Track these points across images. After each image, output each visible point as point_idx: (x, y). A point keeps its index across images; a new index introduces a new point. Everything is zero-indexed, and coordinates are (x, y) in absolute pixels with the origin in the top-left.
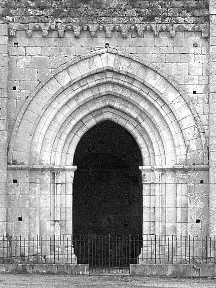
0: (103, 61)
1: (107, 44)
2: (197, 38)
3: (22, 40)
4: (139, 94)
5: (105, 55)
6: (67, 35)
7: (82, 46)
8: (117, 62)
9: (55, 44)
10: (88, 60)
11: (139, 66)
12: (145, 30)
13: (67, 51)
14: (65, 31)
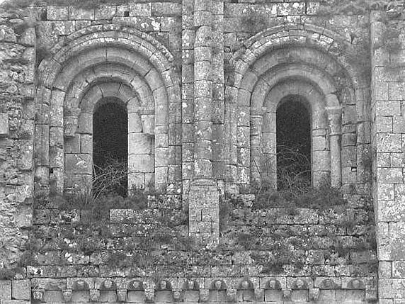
12: (268, 288)
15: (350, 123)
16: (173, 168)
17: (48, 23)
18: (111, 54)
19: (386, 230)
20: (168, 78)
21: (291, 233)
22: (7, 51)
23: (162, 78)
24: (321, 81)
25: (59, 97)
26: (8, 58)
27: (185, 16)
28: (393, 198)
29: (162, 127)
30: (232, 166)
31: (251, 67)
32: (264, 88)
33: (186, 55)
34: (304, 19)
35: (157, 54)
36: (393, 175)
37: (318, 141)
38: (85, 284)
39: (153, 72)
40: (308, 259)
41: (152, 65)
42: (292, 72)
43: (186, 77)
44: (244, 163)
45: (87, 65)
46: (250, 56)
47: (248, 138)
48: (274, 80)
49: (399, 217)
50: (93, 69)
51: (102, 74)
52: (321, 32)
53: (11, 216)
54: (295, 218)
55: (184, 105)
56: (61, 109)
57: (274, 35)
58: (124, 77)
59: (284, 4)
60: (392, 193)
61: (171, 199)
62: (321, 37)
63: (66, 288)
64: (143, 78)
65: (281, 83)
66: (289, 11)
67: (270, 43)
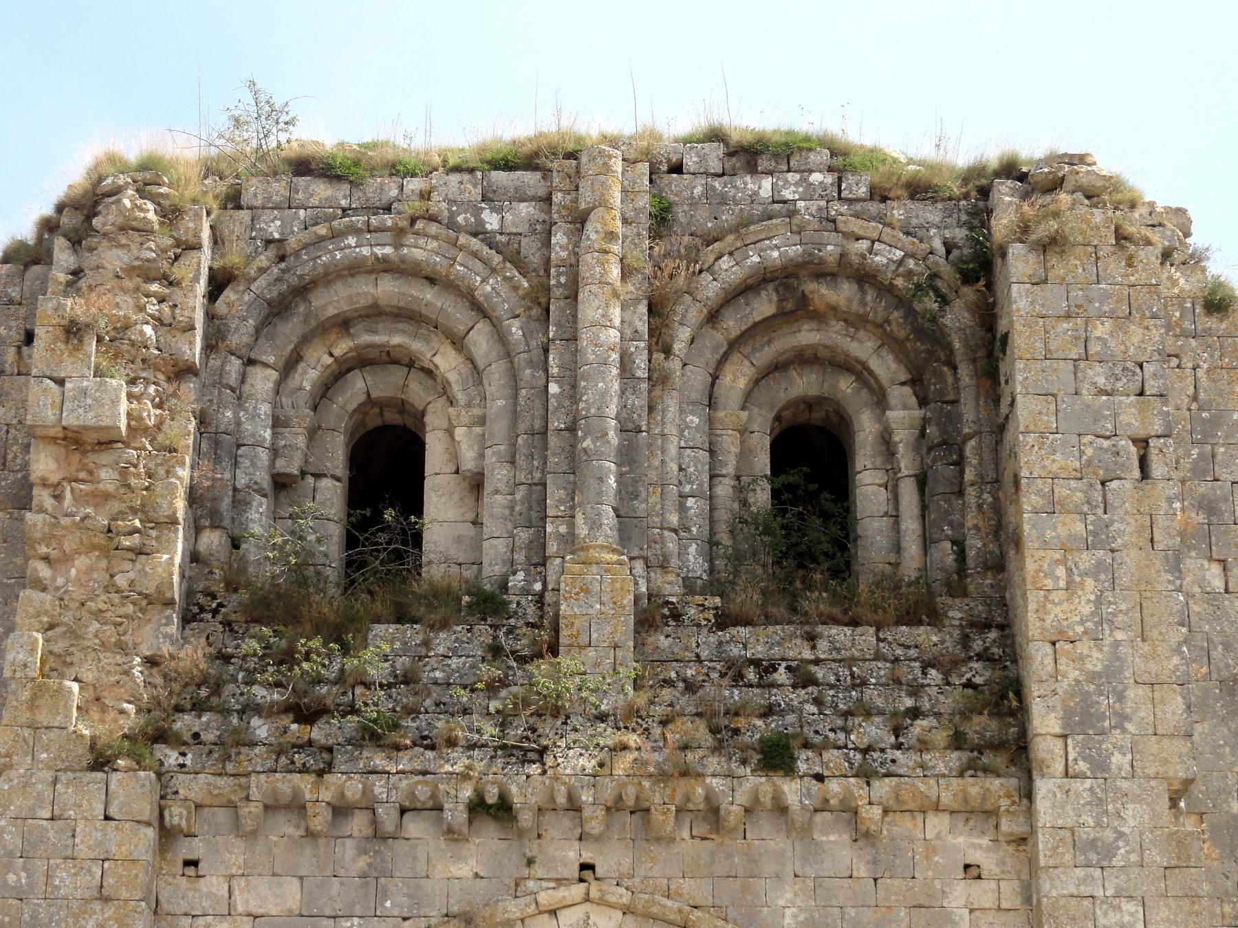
1: (585, 867)
2: (977, 841)
3: (223, 855)
4: (516, 389)
6: (415, 827)
7: (477, 875)
13: (409, 896)
14: (403, 811)
15: (945, 442)
16: (524, 535)
17: (245, 215)
18: (387, 289)
19: (1049, 661)
21: (809, 681)
22: (133, 247)
23: (501, 337)
24: (875, 357)
25: (262, 381)
26: (137, 263)
28: (1062, 584)
29: (502, 447)
30: (666, 533)
31: (713, 317)
32: (737, 378)
33: (557, 279)
34: (836, 207)
36: (1062, 531)
37: (869, 487)
38: (296, 794)
39: (482, 326)
40: (853, 737)
41: (481, 310)
42: (807, 336)
43: (559, 325)
44: (694, 530)
45: (331, 311)
46: (710, 288)
47: (706, 479)
48: (766, 355)
49: (1080, 629)
50: (344, 324)
51: (366, 338)
53: (121, 624)
55: (554, 388)
56: (265, 409)
57: (767, 242)
58: (416, 346)
60: (1061, 572)
61: (518, 603)
62: (877, 245)
63: (247, 798)
64: (458, 343)
65: (778, 367)
66: (801, 189)
67: (756, 259)
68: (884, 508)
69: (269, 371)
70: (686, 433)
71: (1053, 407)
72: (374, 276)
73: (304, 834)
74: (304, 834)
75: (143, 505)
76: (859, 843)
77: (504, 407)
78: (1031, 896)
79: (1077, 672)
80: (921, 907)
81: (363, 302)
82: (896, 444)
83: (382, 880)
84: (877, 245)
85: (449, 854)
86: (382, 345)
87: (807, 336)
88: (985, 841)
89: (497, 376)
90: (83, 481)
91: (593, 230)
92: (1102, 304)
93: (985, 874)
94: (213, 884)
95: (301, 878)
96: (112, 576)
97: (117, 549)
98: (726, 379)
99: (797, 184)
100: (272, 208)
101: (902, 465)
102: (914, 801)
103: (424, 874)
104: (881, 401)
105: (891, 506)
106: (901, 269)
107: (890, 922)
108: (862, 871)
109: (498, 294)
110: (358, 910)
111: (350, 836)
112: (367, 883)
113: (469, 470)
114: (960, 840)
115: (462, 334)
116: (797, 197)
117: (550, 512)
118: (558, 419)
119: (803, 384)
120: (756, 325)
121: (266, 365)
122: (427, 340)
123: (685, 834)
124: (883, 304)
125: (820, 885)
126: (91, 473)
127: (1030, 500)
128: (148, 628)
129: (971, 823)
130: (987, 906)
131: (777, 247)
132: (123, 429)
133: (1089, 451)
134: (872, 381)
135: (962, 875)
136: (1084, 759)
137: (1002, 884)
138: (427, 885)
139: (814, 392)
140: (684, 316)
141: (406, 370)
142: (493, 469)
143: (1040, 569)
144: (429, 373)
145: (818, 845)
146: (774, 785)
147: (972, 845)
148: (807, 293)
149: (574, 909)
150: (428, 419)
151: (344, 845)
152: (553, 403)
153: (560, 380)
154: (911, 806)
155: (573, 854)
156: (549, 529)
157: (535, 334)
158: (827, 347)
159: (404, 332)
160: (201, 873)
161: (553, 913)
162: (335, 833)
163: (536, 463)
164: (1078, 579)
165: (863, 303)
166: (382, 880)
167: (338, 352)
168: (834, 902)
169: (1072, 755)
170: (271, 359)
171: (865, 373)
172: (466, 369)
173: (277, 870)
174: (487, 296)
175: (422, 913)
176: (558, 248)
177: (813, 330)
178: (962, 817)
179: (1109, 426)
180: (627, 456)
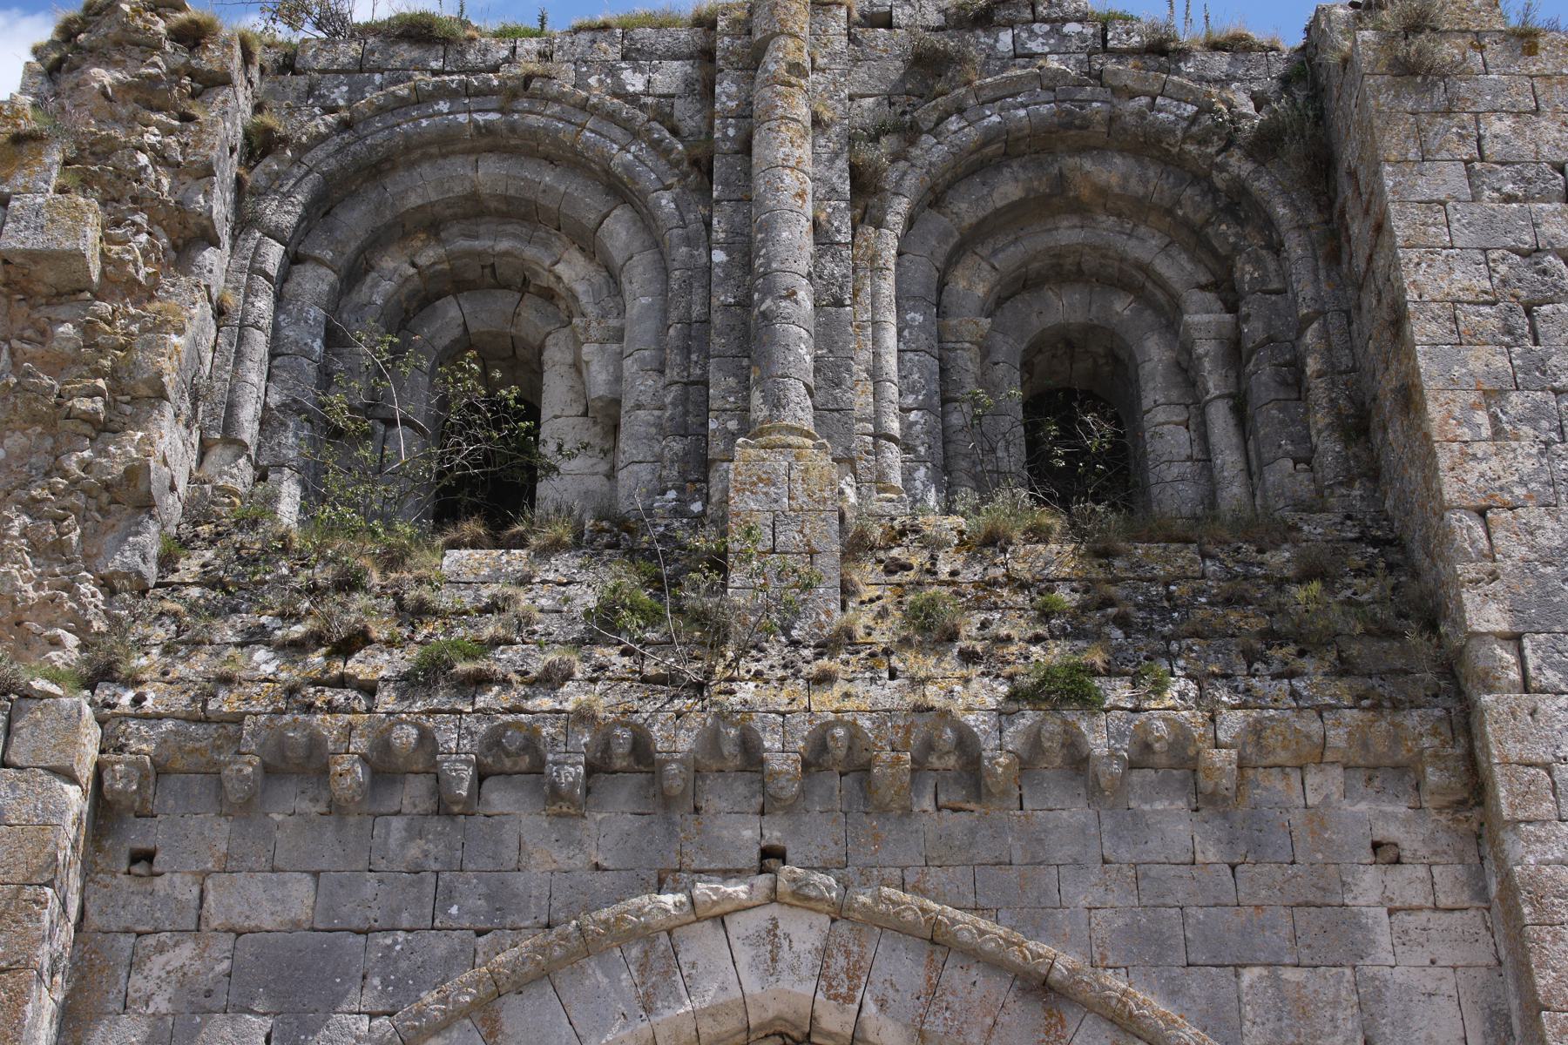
0: (744, 955)
2: (1389, 808)
5: (756, 921)
6: (499, 798)
7: (597, 867)
8: (842, 961)
9: (414, 851)
10: (635, 952)
11: (997, 988)
12: (1027, 763)
13: (489, 897)
15: (1270, 339)
18: (490, 174)
20: (666, 202)
23: (646, 219)
27: (726, 39)
28: (1486, 432)
29: (647, 353)
31: (934, 198)
32: (973, 284)
35: (633, 149)
41: (619, 190)
42: (1067, 233)
43: (726, 184)
44: (922, 450)
45: (414, 200)
46: (932, 152)
48: (1012, 254)
49: (1520, 491)
50: (432, 224)
51: (463, 244)
52: (1156, 87)
54: (1117, 563)
56: (315, 313)
59: (1036, 26)
60: (1481, 417)
64: (588, 243)
67: (996, 119)
68: (1186, 451)
69: (323, 271)
70: (906, 333)
71: (1441, 218)
72: (473, 158)
73: (324, 810)
74: (324, 810)
75: (114, 370)
76: (1203, 813)
77: (652, 304)
78: (1485, 888)
79: (1524, 549)
80: (1308, 904)
81: (458, 189)
82: (1199, 358)
83: (446, 876)
84: (1159, 100)
85: (554, 837)
86: (479, 254)
87: (1067, 233)
88: (1401, 809)
89: (640, 269)
90: (30, 341)
91: (774, 64)
92: (1495, 96)
93: (1406, 855)
94: (176, 885)
95: (316, 874)
96: (57, 458)
97: (67, 418)
98: (960, 282)
99: (1046, 35)
100: (337, 72)
101: (1211, 385)
102: (1285, 748)
103: (513, 865)
104: (1170, 316)
105: (1196, 449)
106: (1195, 129)
107: (1262, 928)
108: (1210, 853)
109: (643, 163)
110: (405, 920)
111: (398, 813)
112: (422, 881)
113: (600, 398)
114: (1362, 806)
115: (592, 225)
116: (1047, 49)
117: (714, 404)
118: (725, 293)
119: (1063, 308)
120: (998, 213)
121: (319, 262)
122: (546, 245)
123: (927, 803)
124: (1171, 180)
125: (1145, 876)
126: (43, 333)
127: (1422, 329)
128: (109, 537)
129: (1377, 783)
130: (1415, 902)
131: (1024, 106)
132: (95, 278)
133: (1503, 269)
134: (1159, 295)
135: (1371, 859)
136: (1551, 666)
137: (1436, 870)
138: (518, 881)
139: (1078, 317)
140: (898, 184)
141: (518, 296)
142: (634, 380)
143: (1450, 415)
144: (549, 295)
145: (1138, 817)
146: (1065, 722)
147: (1390, 816)
148: (1065, 171)
149: (752, 913)
150: (546, 356)
151: (388, 825)
152: (718, 272)
153: (727, 247)
154: (1282, 756)
155: (748, 834)
156: (712, 425)
157: (692, 207)
158: (1095, 248)
159: (515, 236)
160: (156, 869)
161: (721, 919)
162: (375, 809)
163: (694, 357)
164: (1508, 428)
165: (1144, 181)
166: (446, 876)
167: (424, 260)
168: (1169, 900)
169: (1532, 661)
170: (329, 255)
171: (1149, 285)
172: (599, 278)
173: (278, 863)
174: (627, 168)
175: (508, 922)
176: (724, 99)
177: (1075, 227)
178: (1361, 775)
179: (1527, 238)
180: (827, 334)
